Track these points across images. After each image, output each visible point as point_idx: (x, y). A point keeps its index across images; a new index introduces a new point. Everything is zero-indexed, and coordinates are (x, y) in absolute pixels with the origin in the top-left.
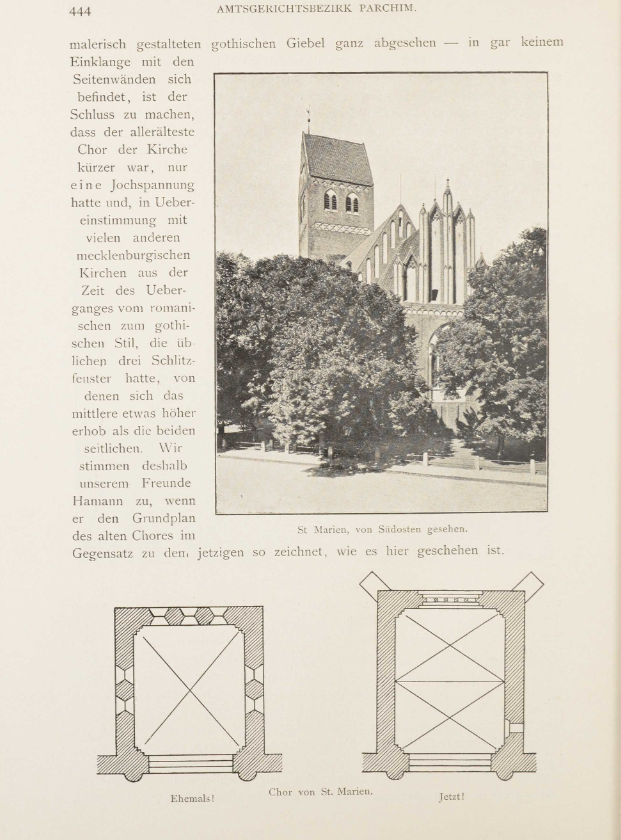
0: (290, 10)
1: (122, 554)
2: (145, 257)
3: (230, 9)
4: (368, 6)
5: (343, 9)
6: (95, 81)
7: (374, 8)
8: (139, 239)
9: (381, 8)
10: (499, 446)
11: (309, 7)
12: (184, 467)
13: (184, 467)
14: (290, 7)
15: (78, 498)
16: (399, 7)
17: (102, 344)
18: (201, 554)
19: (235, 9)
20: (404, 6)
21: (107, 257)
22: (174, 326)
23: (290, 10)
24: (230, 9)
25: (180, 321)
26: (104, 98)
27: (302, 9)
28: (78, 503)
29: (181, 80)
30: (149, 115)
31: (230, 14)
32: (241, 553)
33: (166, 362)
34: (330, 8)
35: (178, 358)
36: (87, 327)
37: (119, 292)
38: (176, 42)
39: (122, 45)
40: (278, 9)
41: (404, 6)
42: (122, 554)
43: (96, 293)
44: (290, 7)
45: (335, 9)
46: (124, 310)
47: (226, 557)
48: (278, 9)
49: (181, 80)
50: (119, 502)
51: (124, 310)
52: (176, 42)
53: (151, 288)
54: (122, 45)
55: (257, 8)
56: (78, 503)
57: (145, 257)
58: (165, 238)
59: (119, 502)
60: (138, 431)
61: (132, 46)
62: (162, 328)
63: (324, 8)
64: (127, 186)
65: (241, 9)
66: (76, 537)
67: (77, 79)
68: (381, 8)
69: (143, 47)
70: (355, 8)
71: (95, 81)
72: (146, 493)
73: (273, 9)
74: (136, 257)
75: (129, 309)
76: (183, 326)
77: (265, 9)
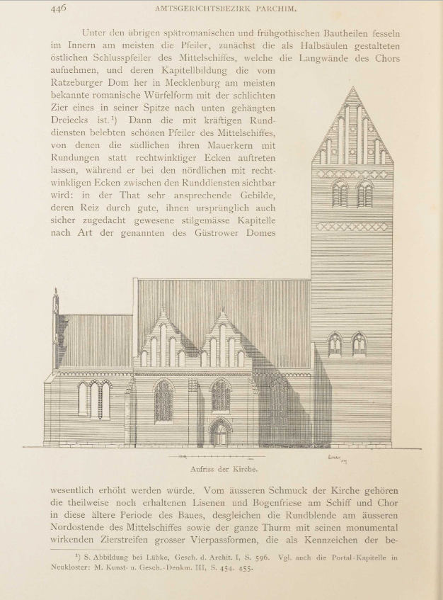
2: (214, 84)
4: (262, 8)
5: (244, 9)
7: (266, 9)
11: (220, 8)
14: (281, 8)
19: (168, 8)
21: (188, 84)
23: (207, 9)
26: (69, 71)
31: (164, 12)
32: (317, 34)
33: (342, 541)
34: (235, 9)
36: (303, 34)
38: (261, 219)
39: (128, 209)
44: (281, 8)
45: (239, 9)
46: (55, 147)
51: (55, 147)
52: (261, 219)
54: (128, 209)
55: (184, 8)
57: (214, 84)
61: (227, 491)
63: (231, 9)
64: (129, 504)
65: (172, 8)
67: (54, 83)
73: (195, 9)
75: (58, 146)
76: (273, 221)
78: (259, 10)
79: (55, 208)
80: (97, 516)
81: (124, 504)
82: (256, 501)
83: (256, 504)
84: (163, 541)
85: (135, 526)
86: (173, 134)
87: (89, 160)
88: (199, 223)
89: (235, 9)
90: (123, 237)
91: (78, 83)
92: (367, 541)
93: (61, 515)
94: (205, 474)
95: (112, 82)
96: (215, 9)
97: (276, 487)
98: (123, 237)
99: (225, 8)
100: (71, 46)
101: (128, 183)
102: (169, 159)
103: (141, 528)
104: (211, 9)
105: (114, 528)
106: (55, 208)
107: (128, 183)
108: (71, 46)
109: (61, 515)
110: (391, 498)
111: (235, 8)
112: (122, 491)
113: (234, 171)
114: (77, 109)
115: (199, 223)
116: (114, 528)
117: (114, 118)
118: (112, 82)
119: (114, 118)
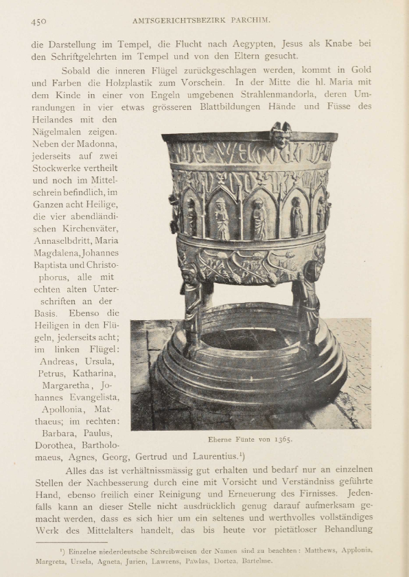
0: (255, 21)
1: (238, 530)
2: (58, 387)
4: (237, 18)
6: (246, 57)
7: (241, 20)
8: (40, 108)
9: (246, 20)
11: (196, 20)
14: (255, 19)
16: (258, 19)
17: (344, 95)
20: (262, 19)
23: (255, 21)
27: (191, 21)
30: (37, 458)
31: (141, 24)
34: (211, 20)
40: (174, 21)
41: (262, 19)
42: (238, 530)
43: (64, 327)
48: (174, 21)
49: (96, 193)
50: (72, 108)
51: (324, 519)
53: (73, 560)
55: (161, 20)
59: (72, 108)
60: (65, 144)
63: (207, 20)
68: (246, 20)
69: (365, 507)
70: (228, 20)
71: (246, 57)
72: (73, 428)
73: (171, 21)
74: (176, 495)
75: (260, 530)
77: (166, 20)
83: (328, 530)
84: (161, 108)
85: (277, 80)
91: (212, 95)
92: (101, 302)
95: (39, 445)
99: (201, 20)
100: (239, 83)
101: (103, 156)
102: (175, 495)
103: (283, 83)
104: (187, 21)
105: (255, 82)
107: (103, 156)
108: (239, 83)
111: (211, 20)
116: (255, 82)
118: (39, 445)
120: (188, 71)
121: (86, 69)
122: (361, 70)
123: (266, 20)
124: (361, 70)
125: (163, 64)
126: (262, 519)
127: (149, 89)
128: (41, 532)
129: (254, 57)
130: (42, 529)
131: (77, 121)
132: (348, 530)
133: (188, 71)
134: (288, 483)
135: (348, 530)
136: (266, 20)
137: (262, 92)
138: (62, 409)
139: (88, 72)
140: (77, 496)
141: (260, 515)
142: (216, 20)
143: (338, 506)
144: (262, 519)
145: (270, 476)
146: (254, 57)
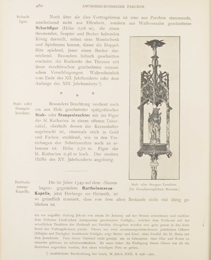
3: (87, 6)
4: (130, 6)
5: (122, 7)
10: (144, 104)
12: (66, 127)
13: (66, 127)
14: (138, 6)
15: (55, 108)
18: (175, 216)
19: (88, 6)
20: (141, 6)
22: (107, 194)
24: (87, 6)
25: (54, 131)
28: (55, 110)
29: (67, 23)
34: (118, 7)
35: (65, 72)
37: (102, 116)
40: (101, 6)
44: (138, 6)
47: (108, 249)
48: (101, 6)
49: (67, 23)
55: (95, 6)
56: (55, 110)
58: (66, 104)
62: (101, 111)
63: (116, 7)
65: (90, 6)
66: (87, 62)
70: (126, 7)
77: (97, 6)
78: (129, 7)
79: (37, 67)
80: (118, 200)
81: (98, 143)
82: (97, 50)
86: (100, 225)
87: (101, 161)
88: (42, 133)
89: (118, 7)
90: (185, 201)
93: (99, 138)
94: (136, 249)
96: (109, 7)
97: (20, 15)
98: (185, 201)
101: (106, 154)
104: (107, 7)
106: (37, 67)
107: (106, 154)
109: (99, 138)
110: (39, 81)
112: (122, 216)
113: (166, 234)
114: (48, 23)
115: (42, 133)
117: (100, 83)
119: (100, 83)
120: (108, 143)
121: (117, 131)
122: (114, 132)
123: (143, 7)
124: (114, 132)
125: (100, 236)
126: (57, 23)
127: (51, 227)
128: (141, 24)
129: (123, 23)
130: (142, 22)
131: (125, 239)
132: (87, 84)
133: (108, 143)
134: (96, 18)
135: (87, 84)
136: (143, 7)
137: (71, 136)
138: (149, 230)
139: (117, 132)
140: (99, 23)
141: (57, 21)
142: (121, 7)
143: (74, 62)
144: (57, 23)
145: (171, 241)
146: (123, 23)
